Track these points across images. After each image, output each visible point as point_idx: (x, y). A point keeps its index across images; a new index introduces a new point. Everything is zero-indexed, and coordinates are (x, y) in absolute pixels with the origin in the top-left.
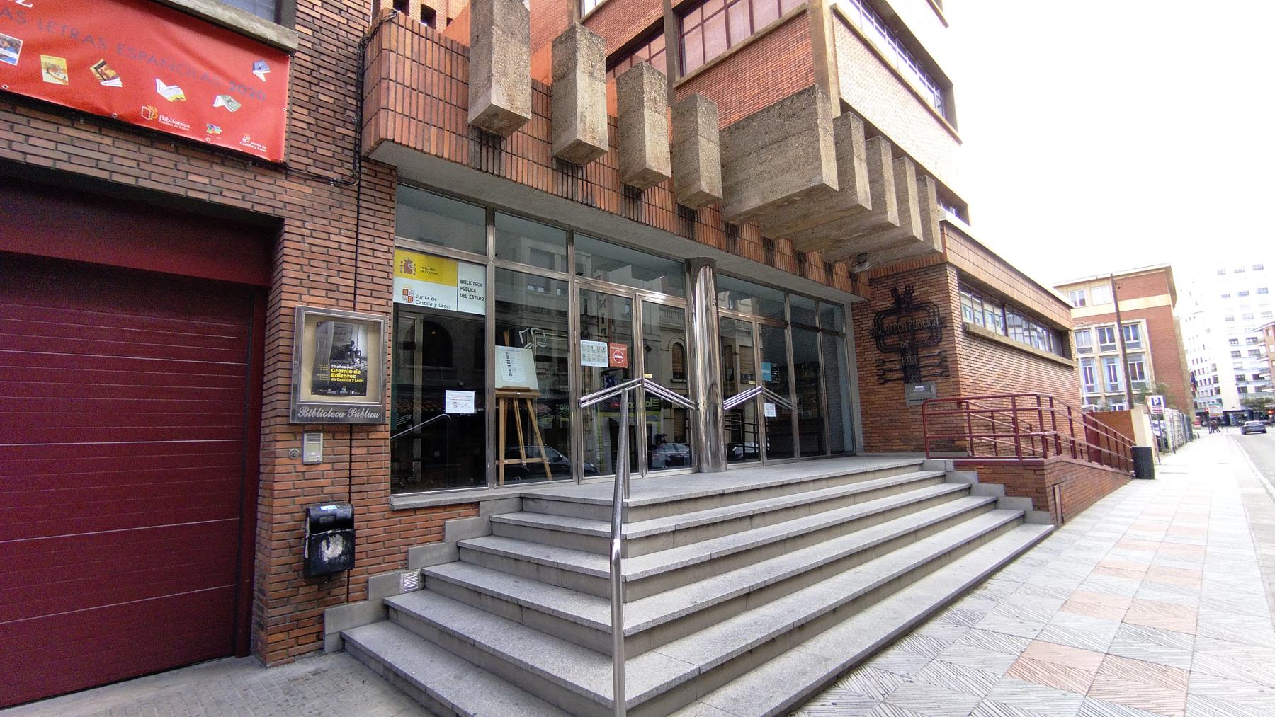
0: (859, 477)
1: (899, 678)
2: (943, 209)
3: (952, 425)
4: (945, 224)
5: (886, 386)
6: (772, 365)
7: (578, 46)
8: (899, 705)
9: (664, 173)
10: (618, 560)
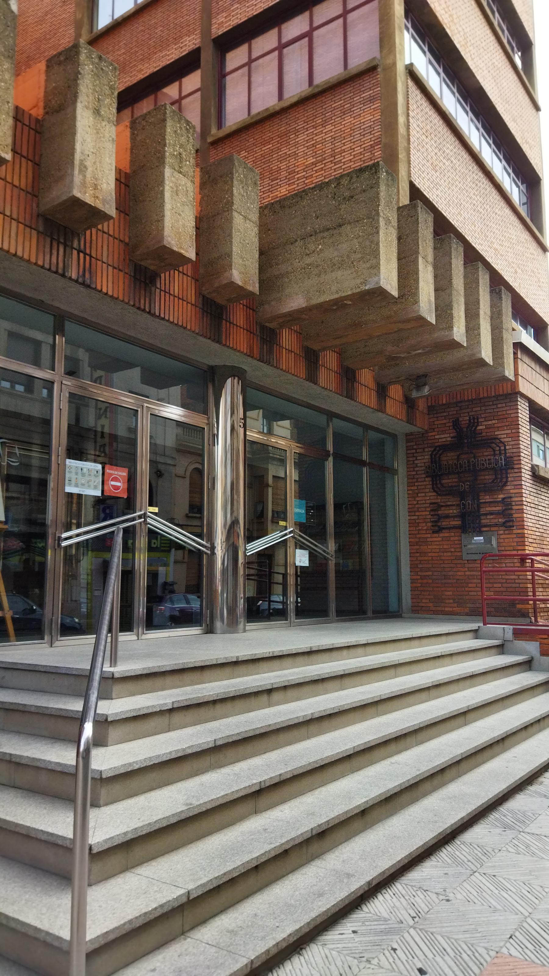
0: (403, 644)
1: (434, 896)
2: (520, 327)
3: (514, 585)
4: (519, 346)
5: (441, 535)
6: (307, 503)
7: (82, 72)
8: (431, 930)
9: (187, 255)
10: (87, 751)
